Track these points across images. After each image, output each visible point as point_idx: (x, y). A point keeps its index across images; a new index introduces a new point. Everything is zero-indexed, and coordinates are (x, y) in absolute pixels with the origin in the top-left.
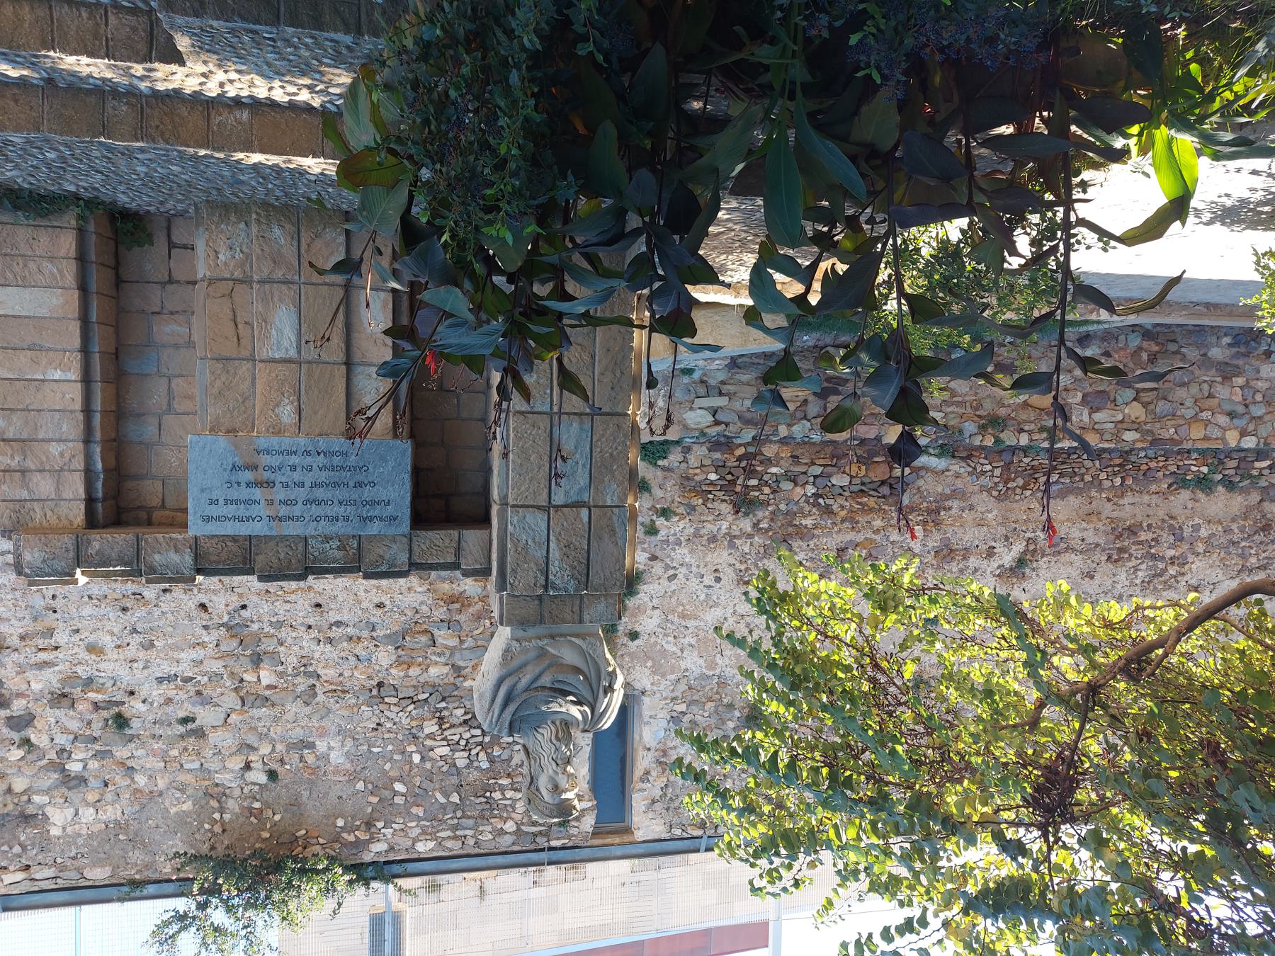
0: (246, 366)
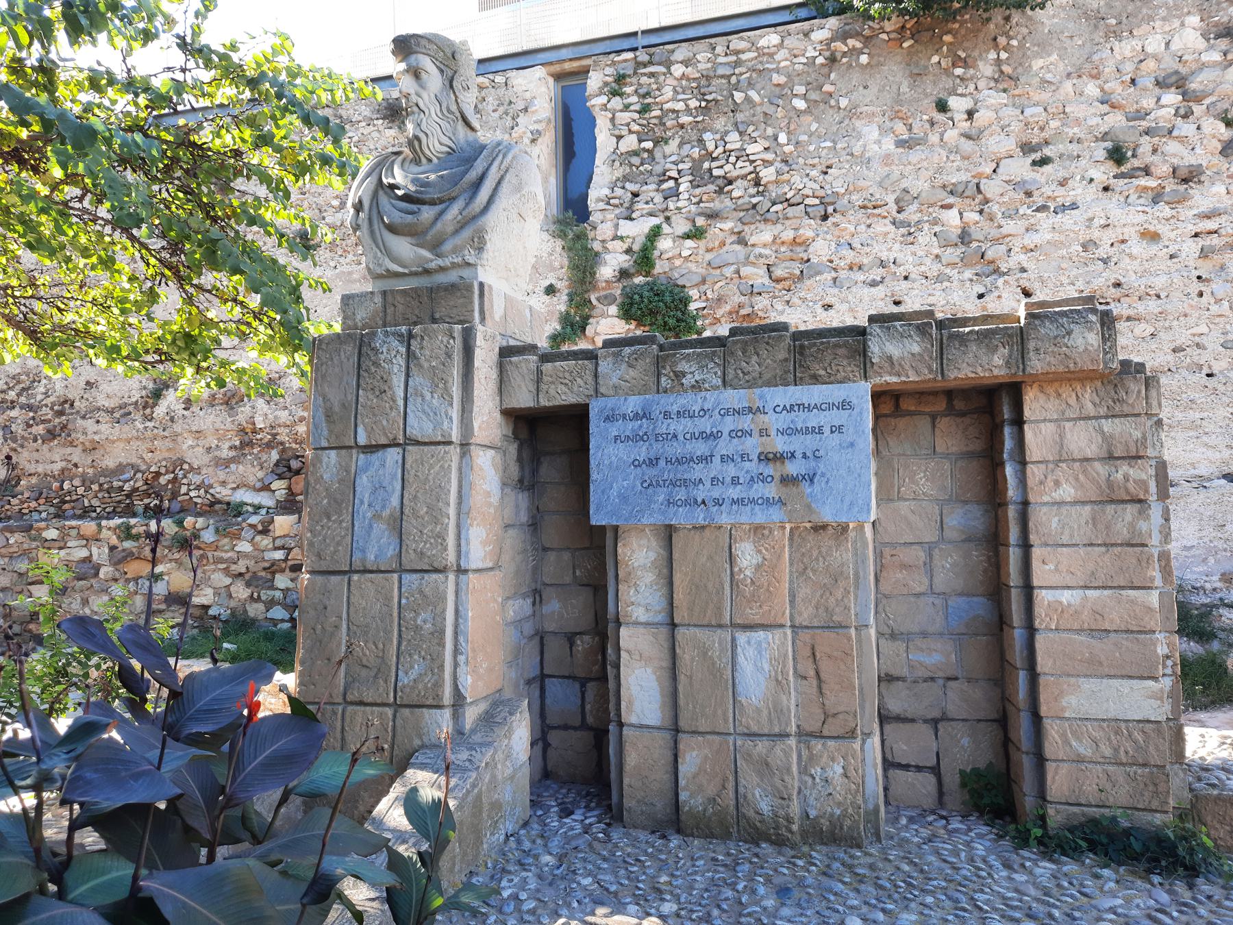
0: (804, 618)
